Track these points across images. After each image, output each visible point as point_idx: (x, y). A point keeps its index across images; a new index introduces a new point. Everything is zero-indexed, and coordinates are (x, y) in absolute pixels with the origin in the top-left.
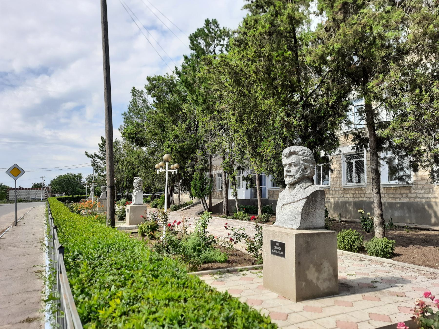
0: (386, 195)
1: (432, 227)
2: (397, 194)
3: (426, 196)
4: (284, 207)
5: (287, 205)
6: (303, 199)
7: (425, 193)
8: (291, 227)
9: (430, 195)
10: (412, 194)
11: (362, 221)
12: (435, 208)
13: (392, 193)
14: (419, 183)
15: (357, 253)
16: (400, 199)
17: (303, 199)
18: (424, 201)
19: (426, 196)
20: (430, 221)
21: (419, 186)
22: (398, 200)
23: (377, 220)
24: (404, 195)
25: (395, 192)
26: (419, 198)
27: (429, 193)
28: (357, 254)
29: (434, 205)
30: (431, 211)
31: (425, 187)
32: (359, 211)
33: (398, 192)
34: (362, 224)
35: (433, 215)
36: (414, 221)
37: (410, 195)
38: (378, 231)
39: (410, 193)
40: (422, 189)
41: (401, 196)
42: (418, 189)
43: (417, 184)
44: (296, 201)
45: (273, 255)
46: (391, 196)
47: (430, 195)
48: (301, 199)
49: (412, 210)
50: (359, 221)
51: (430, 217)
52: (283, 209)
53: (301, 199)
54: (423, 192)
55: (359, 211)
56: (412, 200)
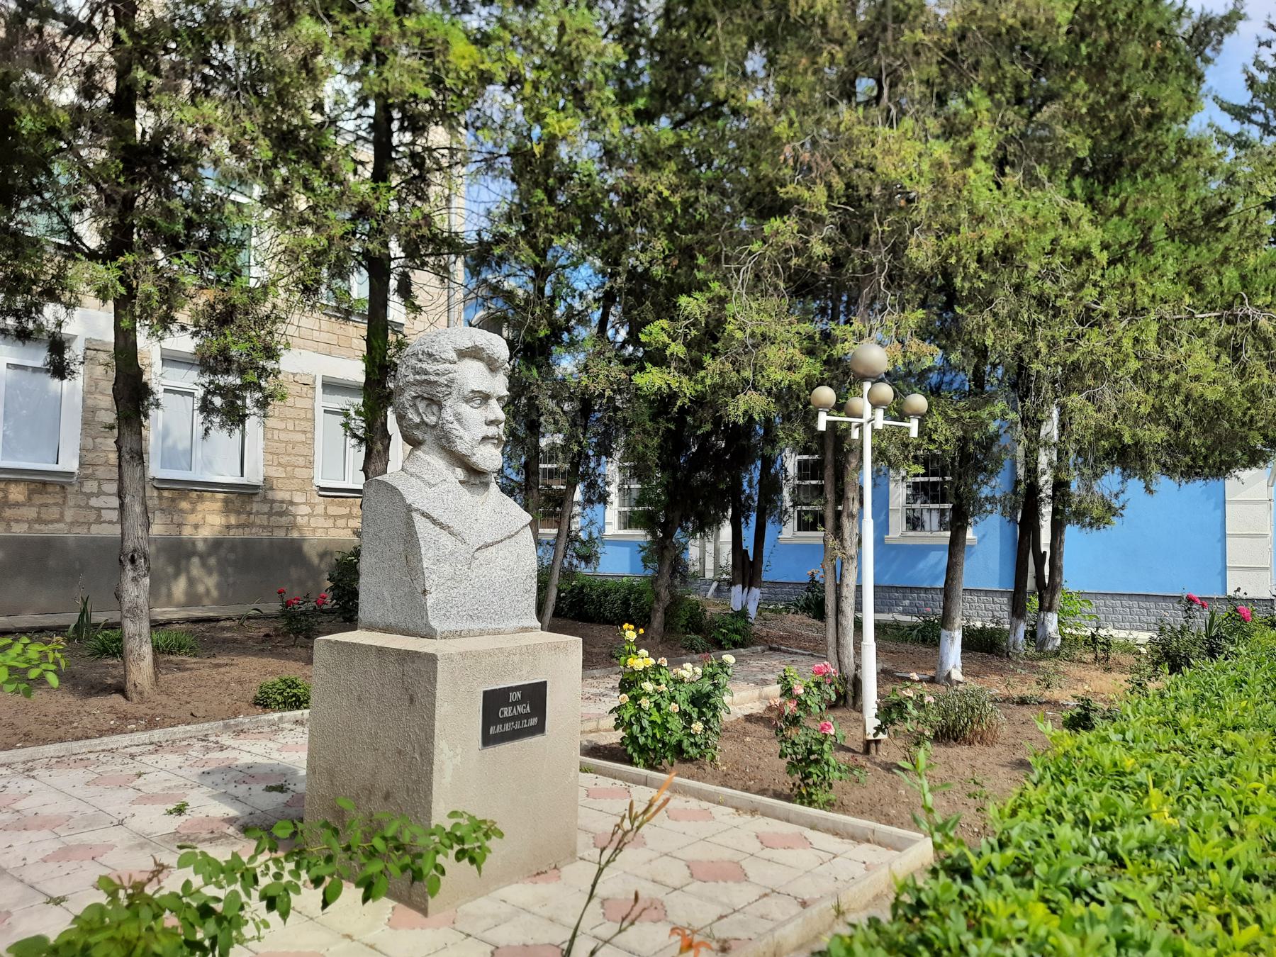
8: (515, 624)
45: (492, 750)
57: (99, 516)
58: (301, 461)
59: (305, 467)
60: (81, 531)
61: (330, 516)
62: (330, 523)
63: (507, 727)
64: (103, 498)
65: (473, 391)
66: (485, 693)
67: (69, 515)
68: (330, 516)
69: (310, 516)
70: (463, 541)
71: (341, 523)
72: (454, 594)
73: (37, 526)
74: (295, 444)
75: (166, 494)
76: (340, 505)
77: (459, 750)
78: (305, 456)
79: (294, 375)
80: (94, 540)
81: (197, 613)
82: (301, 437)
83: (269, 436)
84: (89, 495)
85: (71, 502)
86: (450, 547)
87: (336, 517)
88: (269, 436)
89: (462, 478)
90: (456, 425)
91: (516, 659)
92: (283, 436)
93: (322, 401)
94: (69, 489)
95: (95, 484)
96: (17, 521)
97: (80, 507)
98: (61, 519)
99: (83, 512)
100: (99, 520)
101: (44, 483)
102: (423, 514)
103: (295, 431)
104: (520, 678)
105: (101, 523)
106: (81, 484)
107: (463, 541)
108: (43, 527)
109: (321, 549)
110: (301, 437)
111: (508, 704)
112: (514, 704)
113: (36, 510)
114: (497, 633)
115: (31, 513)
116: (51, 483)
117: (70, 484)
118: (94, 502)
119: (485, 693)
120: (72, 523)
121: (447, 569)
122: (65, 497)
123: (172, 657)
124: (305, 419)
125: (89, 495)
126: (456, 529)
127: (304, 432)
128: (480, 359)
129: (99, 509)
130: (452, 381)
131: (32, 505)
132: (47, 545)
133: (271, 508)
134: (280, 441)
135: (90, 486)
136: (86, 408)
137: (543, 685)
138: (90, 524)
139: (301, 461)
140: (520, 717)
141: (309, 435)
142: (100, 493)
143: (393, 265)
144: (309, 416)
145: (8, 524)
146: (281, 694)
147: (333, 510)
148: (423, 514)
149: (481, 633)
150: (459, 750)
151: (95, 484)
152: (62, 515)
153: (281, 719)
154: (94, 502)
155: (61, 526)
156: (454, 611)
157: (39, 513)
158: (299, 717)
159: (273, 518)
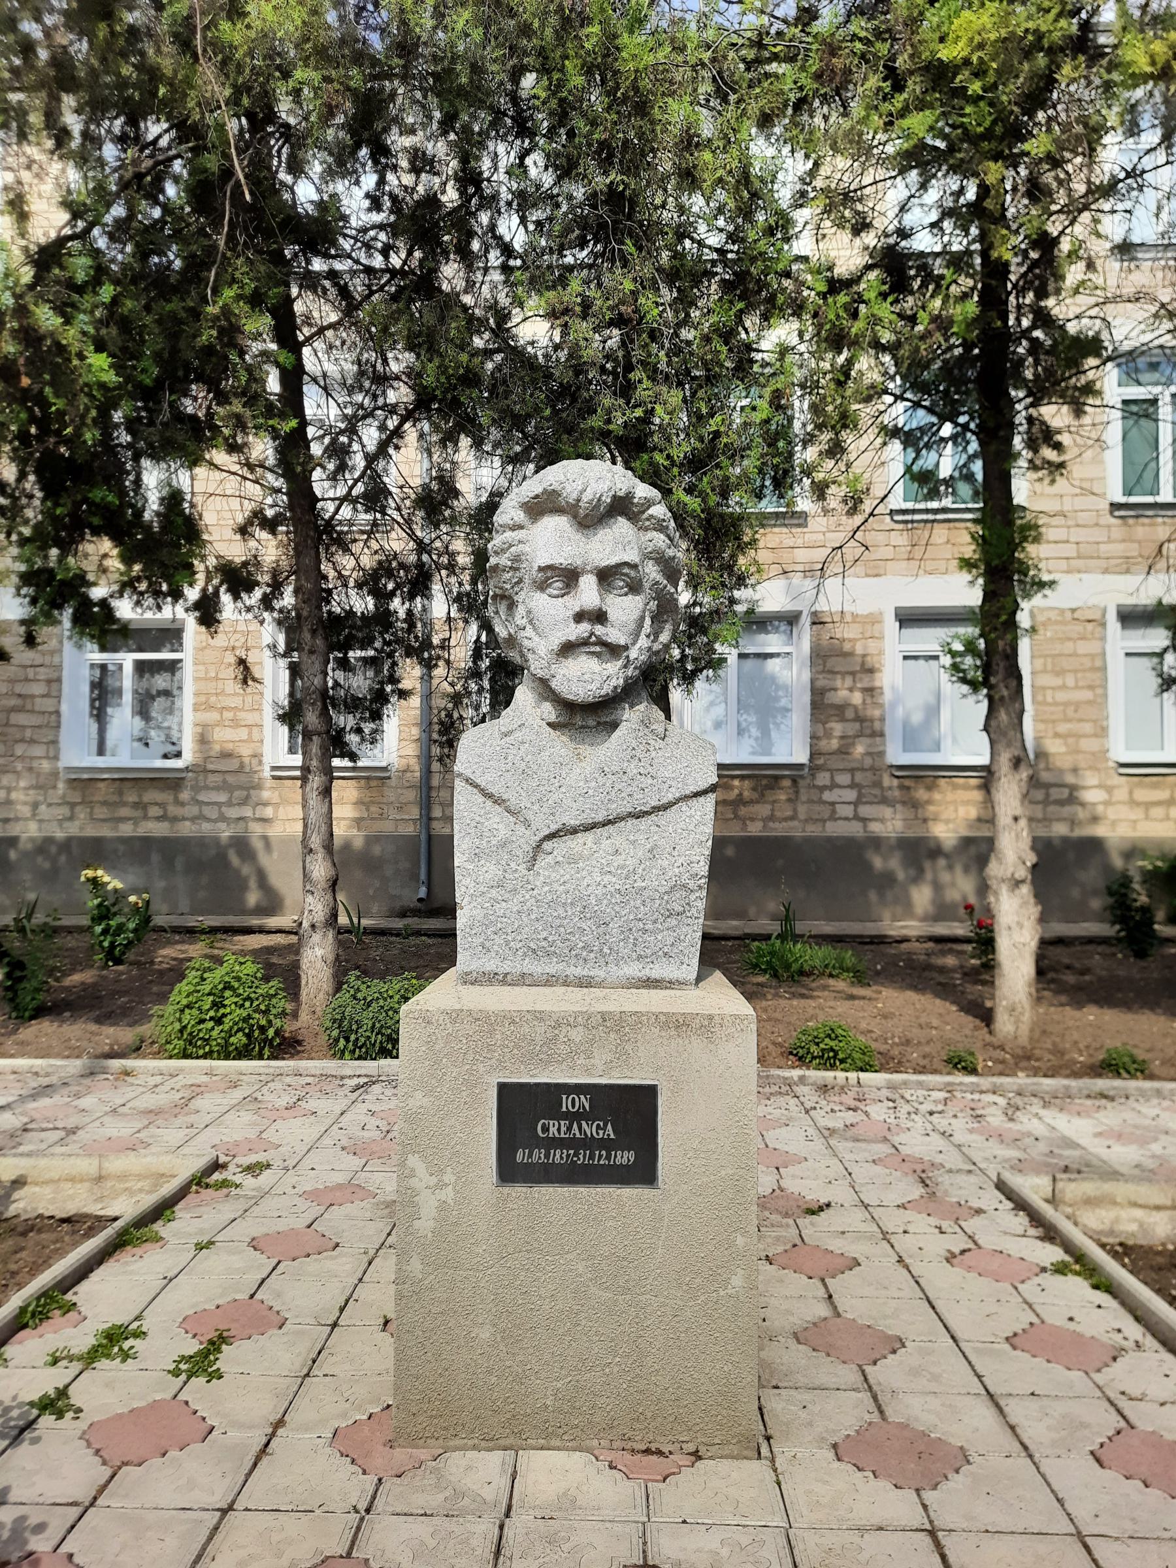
0: (78, 809)
1: (255, 922)
2: (124, 804)
3: (233, 813)
4: (560, 847)
5: (589, 837)
6: (697, 795)
7: (229, 804)
8: (633, 970)
9: (247, 812)
10: (183, 804)
11: (97, 919)
12: (264, 860)
13: (105, 803)
14: (210, 767)
15: (273, 1057)
16: (136, 824)
17: (697, 795)
18: (225, 833)
19: (233, 813)
20: (242, 901)
21: (212, 779)
22: (126, 830)
23: (320, 907)
24: (154, 811)
25: (115, 798)
26: (208, 820)
27: (244, 802)
28: (273, 1063)
29: (258, 845)
30: (246, 870)
31: (230, 779)
32: (90, 873)
33: (131, 798)
34: (98, 929)
35: (253, 883)
36: (184, 904)
37: (173, 810)
38: (319, 952)
39: (179, 803)
40: (217, 788)
41: (138, 813)
42: (207, 788)
43: (206, 771)
44: (657, 809)
45: (518, 1192)
46: (101, 812)
47: (247, 812)
48: (686, 798)
49: (179, 863)
50: (85, 921)
51: (243, 887)
52: (543, 862)
53: (686, 798)
54: (222, 797)
55: (90, 873)
56: (186, 829)
57: (834, 811)
58: (1088, 728)
59: (1096, 735)
60: (813, 830)
61: (1138, 804)
62: (1138, 814)
64: (837, 791)
65: (541, 569)
66: (503, 1088)
67: (802, 810)
68: (1138, 804)
69: (1107, 803)
70: (527, 824)
71: (1157, 812)
72: (500, 908)
74: (1077, 705)
76: (1155, 786)
77: (449, 1177)
78: (1095, 721)
79: (1073, 610)
80: (829, 839)
81: (941, 929)
82: (1087, 695)
83: (1040, 698)
84: (823, 789)
86: (503, 832)
87: (1148, 805)
88: (1040, 698)
89: (553, 718)
90: (529, 632)
91: (577, 1035)
92: (1061, 696)
93: (1118, 640)
94: (802, 783)
95: (827, 775)
96: (752, 819)
99: (817, 808)
100: (833, 817)
101: (777, 778)
103: (1077, 687)
104: (588, 1071)
105: (836, 820)
106: (813, 775)
107: (527, 824)
109: (1127, 846)
110: (1087, 695)
111: (558, 1116)
112: (575, 1117)
113: (769, 807)
114: (585, 983)
115: (764, 810)
116: (784, 777)
117: (802, 777)
118: (827, 796)
119: (503, 1088)
121: (491, 871)
122: (797, 792)
123: (831, 982)
124: (1094, 669)
125: (823, 789)
126: (513, 802)
127: (1091, 687)
128: (559, 510)
129: (833, 804)
130: (517, 559)
132: (781, 845)
133: (1047, 795)
134: (1056, 704)
135: (823, 778)
136: (814, 690)
137: (648, 1094)
138: (824, 821)
139: (1088, 728)
140: (588, 1143)
141: (1099, 691)
142: (834, 786)
143: (1018, 407)
144: (1098, 663)
145: (745, 824)
147: (1142, 795)
149: (549, 981)
150: (449, 1177)
151: (827, 775)
153: (802, 1079)
154: (827, 796)
155: (795, 823)
158: (830, 1082)
159: (1051, 808)
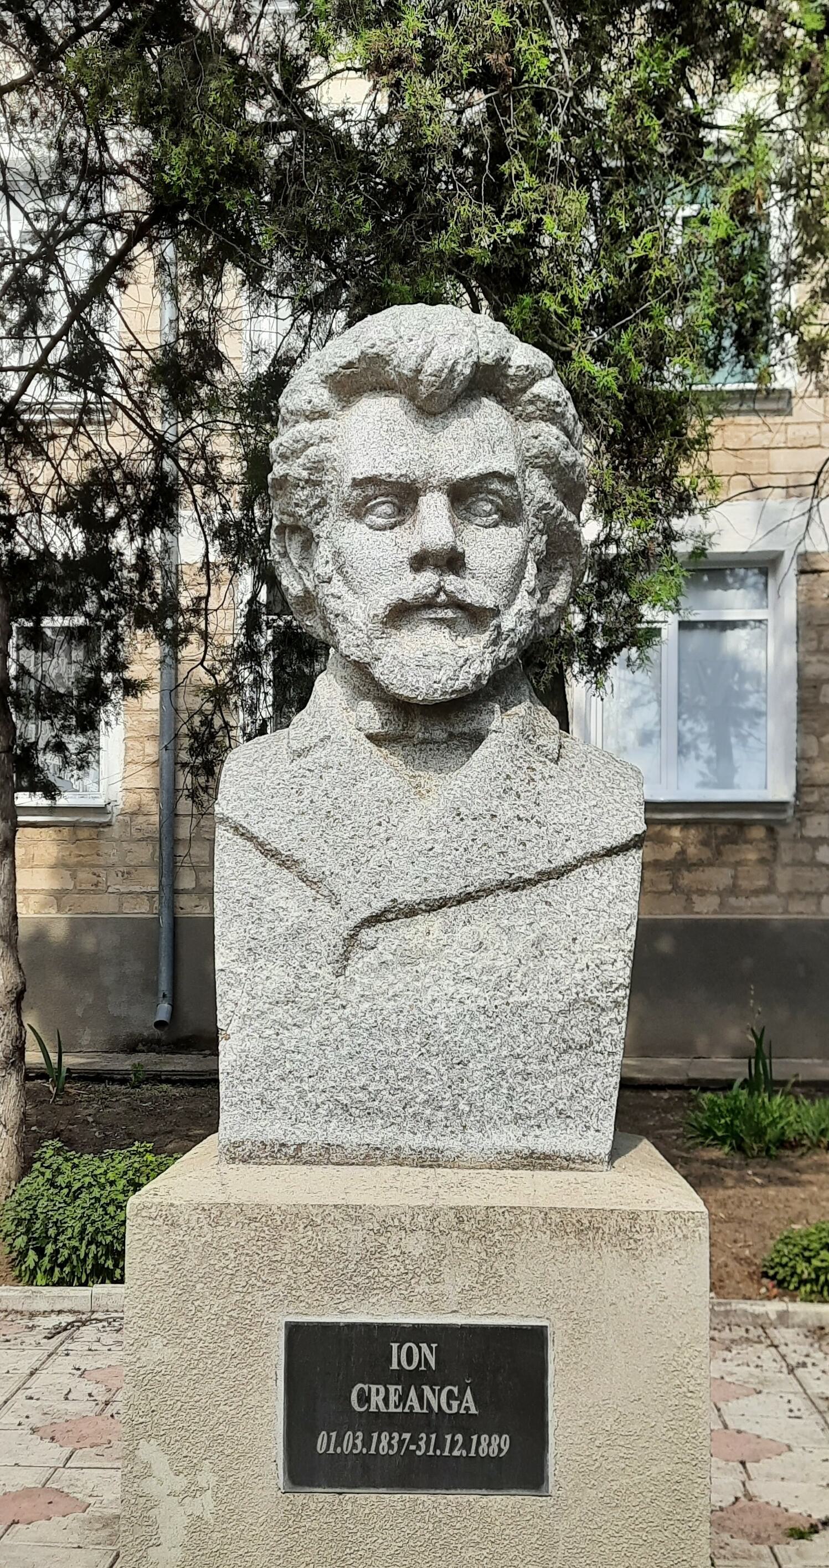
63: (384, 1443)
65: (356, 483)
72: (290, 1038)
73: (732, 900)
75: (84, 833)
77: (206, 1478)
85: (785, 857)
86: (295, 914)
89: (376, 726)
90: (337, 586)
94: (782, 833)
97: (801, 864)
98: (768, 890)
99: (808, 873)
101: (741, 825)
102: (237, 829)
106: (801, 821)
108: (741, 902)
111: (385, 1377)
113: (729, 872)
116: (753, 823)
117: (783, 823)
120: (790, 895)
122: (775, 848)
128: (387, 388)
130: (317, 467)
131: (723, 865)
145: (689, 900)
146: (808, 1260)
148: (237, 829)
150: (206, 1478)
152: (771, 878)
153: (783, 1317)
155: (772, 898)
156: (288, 1090)
157: (735, 877)
